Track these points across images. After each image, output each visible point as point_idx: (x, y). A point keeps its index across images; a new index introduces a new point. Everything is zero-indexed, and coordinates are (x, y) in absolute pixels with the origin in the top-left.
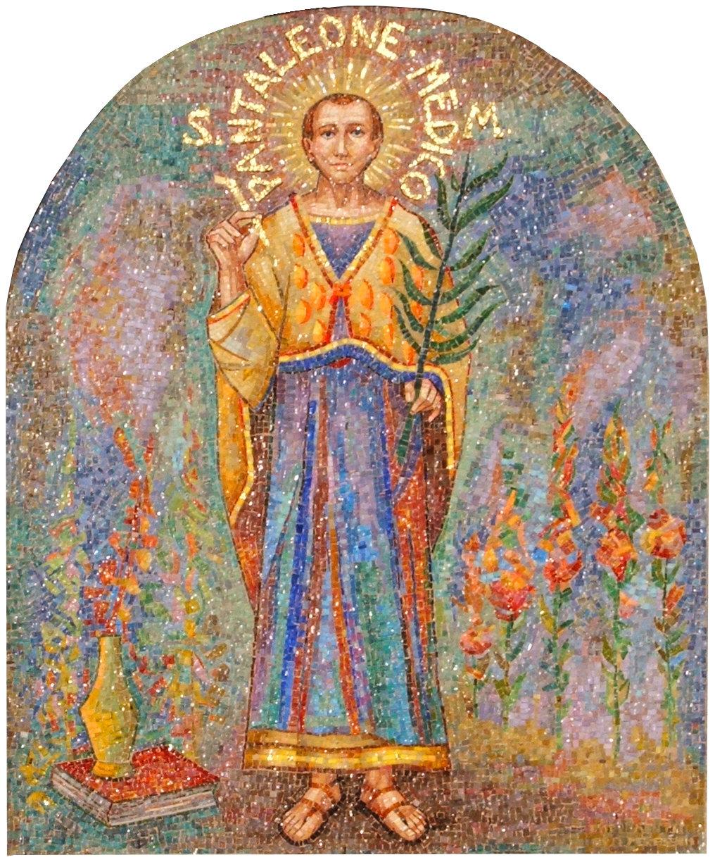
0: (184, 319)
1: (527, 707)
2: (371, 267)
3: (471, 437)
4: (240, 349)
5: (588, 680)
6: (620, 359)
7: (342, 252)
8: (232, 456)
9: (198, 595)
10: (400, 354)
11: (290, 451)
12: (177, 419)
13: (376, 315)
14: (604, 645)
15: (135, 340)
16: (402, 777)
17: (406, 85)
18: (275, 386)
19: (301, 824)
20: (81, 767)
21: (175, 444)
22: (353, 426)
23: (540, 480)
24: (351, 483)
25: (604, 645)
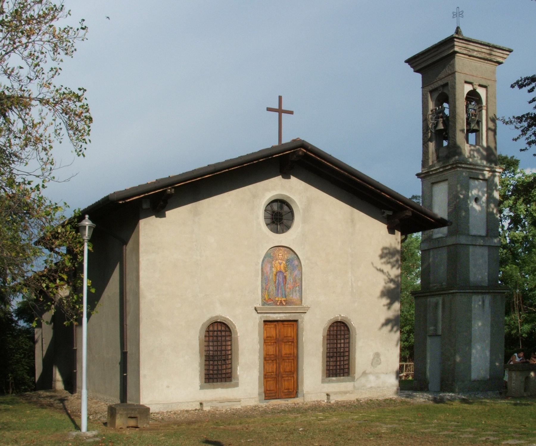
0: (271, 267)
1: (291, 296)
2: (282, 265)
3: (288, 277)
4: (274, 270)
5: (294, 294)
6: (296, 272)
7: (280, 264)
8: (274, 278)
9: (272, 288)
10: (284, 271)
11: (277, 278)
12: (23, 64)
13: (282, 268)
14: (295, 292)
15: (268, 269)
16: (284, 300)
17: (339, 369)
18: (277, 273)
19: (278, 304)
20: (265, 299)
21: (271, 277)
22: (281, 276)
23: (292, 280)
24: (281, 280)
25: (295, 292)
